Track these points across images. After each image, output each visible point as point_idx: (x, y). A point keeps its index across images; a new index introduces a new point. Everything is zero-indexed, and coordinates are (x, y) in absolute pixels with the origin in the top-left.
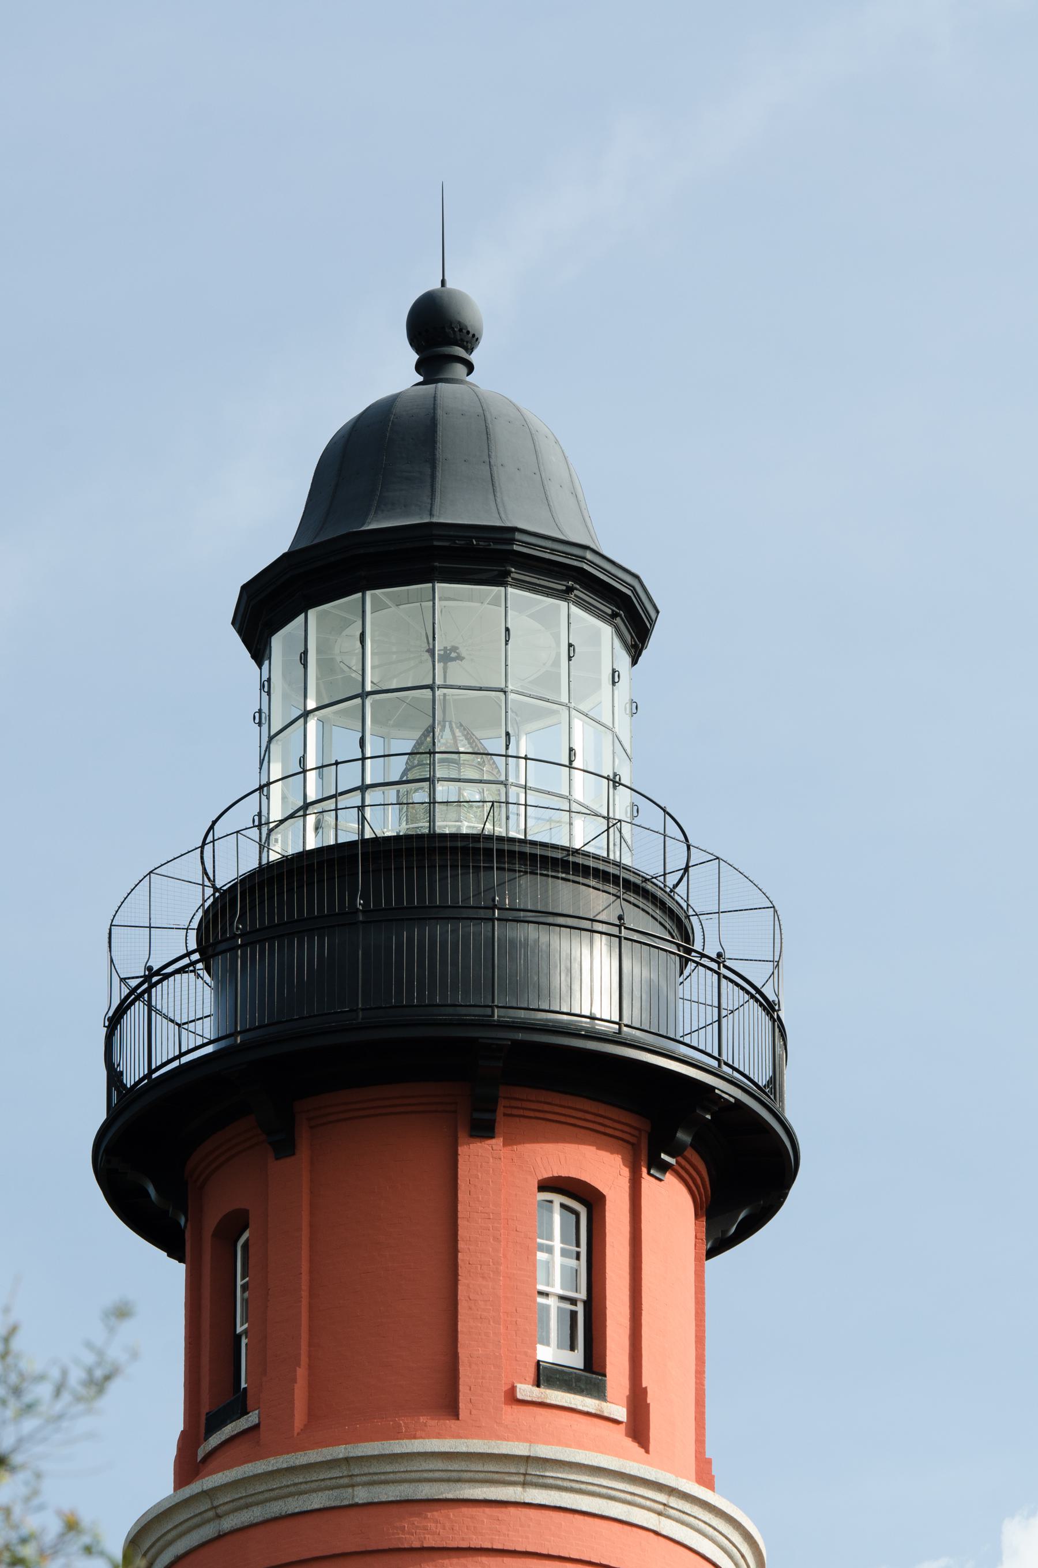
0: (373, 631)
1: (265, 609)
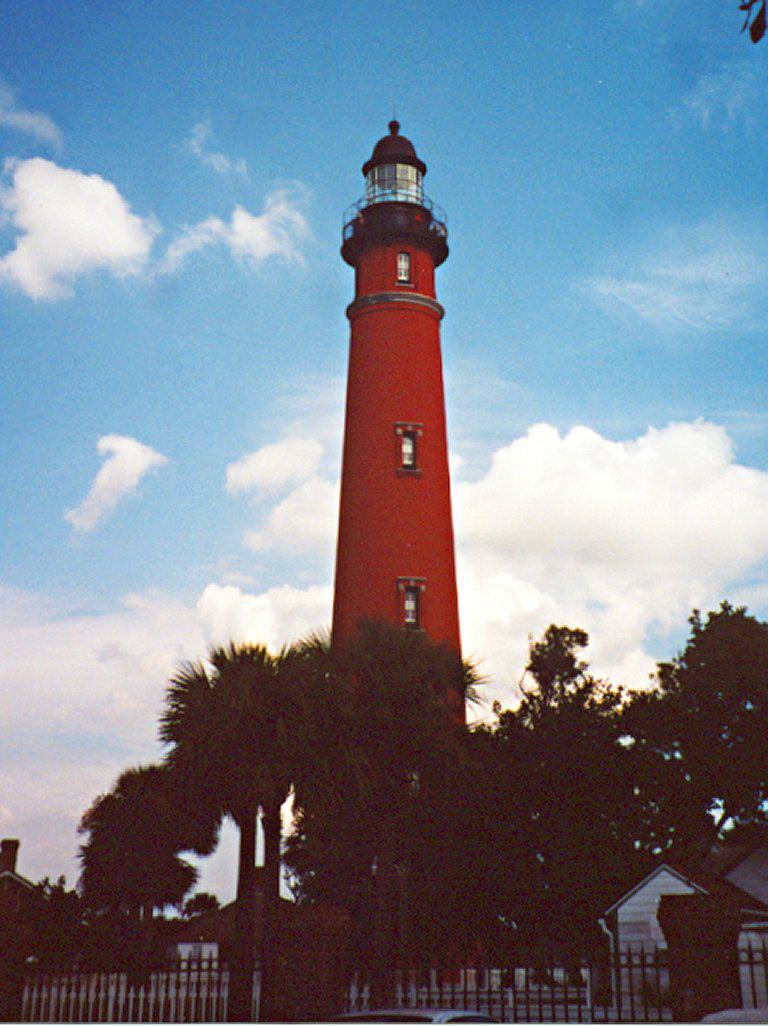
1: (367, 169)
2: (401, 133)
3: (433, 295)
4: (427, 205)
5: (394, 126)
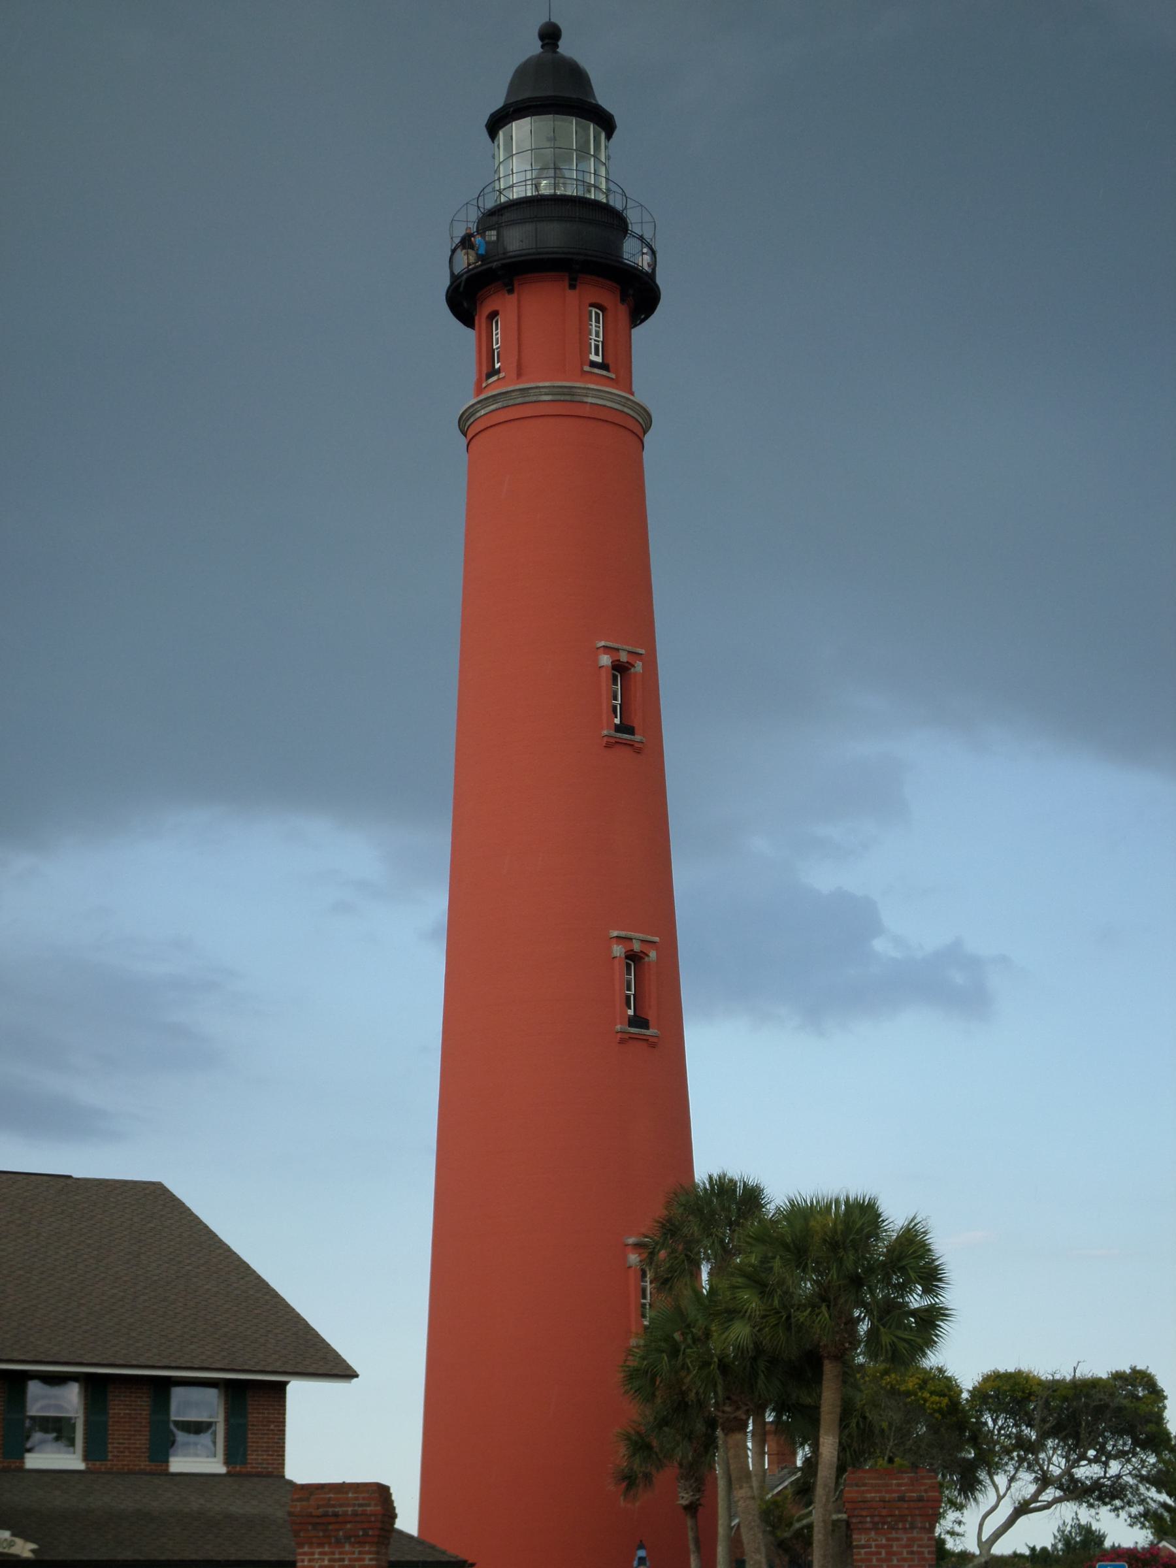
0: (531, 315)
2: (565, 48)
3: (632, 394)
4: (617, 203)
5: (550, 35)
